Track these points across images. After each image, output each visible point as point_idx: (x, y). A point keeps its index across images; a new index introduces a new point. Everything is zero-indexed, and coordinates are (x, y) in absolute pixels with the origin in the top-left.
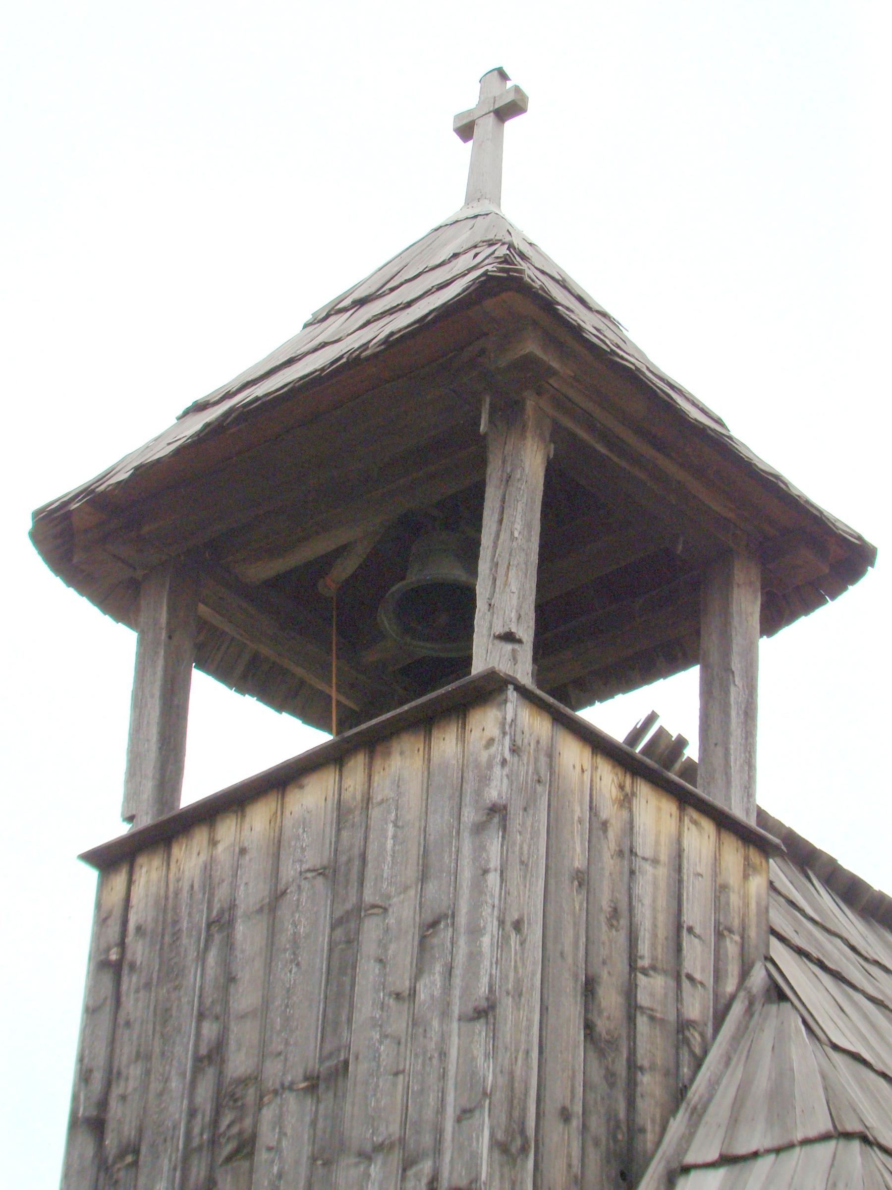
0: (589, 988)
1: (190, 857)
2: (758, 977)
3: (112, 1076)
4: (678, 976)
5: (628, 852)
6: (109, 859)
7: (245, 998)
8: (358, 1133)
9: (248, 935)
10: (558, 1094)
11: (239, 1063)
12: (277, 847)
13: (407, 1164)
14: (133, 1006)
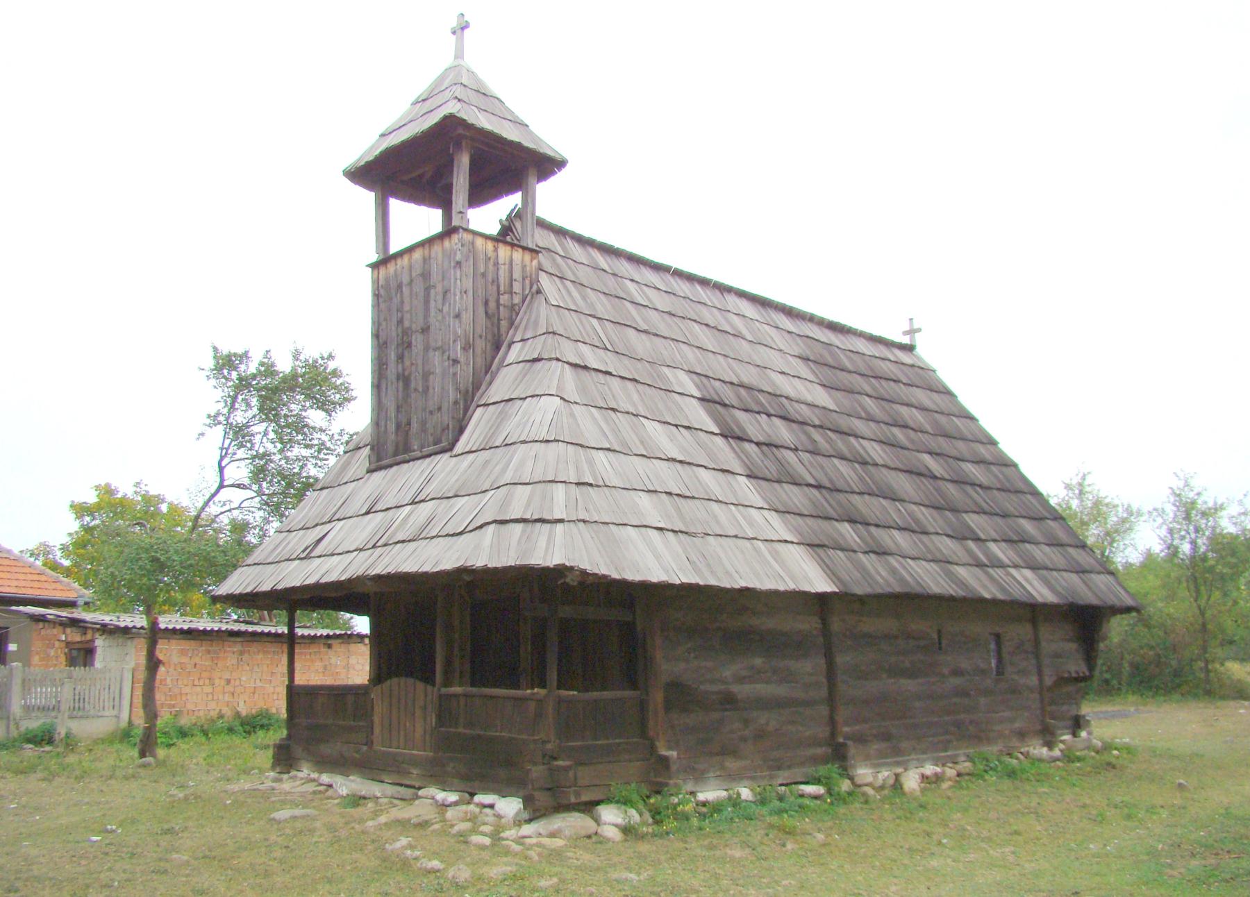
0: (486, 303)
1: (391, 268)
2: (535, 288)
3: (379, 325)
4: (511, 293)
5: (496, 264)
6: (375, 266)
7: (407, 308)
8: (433, 344)
9: (406, 290)
10: (478, 331)
11: (407, 324)
12: (411, 268)
13: (444, 352)
14: (383, 306)
